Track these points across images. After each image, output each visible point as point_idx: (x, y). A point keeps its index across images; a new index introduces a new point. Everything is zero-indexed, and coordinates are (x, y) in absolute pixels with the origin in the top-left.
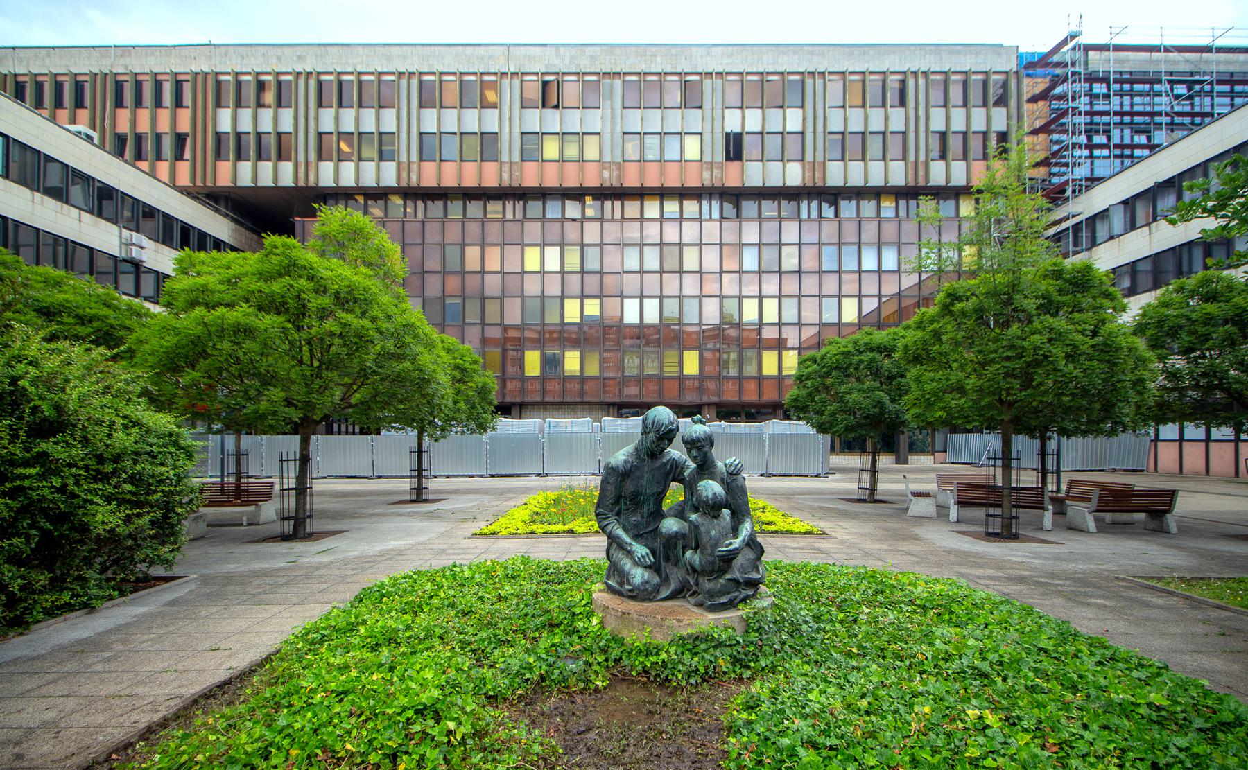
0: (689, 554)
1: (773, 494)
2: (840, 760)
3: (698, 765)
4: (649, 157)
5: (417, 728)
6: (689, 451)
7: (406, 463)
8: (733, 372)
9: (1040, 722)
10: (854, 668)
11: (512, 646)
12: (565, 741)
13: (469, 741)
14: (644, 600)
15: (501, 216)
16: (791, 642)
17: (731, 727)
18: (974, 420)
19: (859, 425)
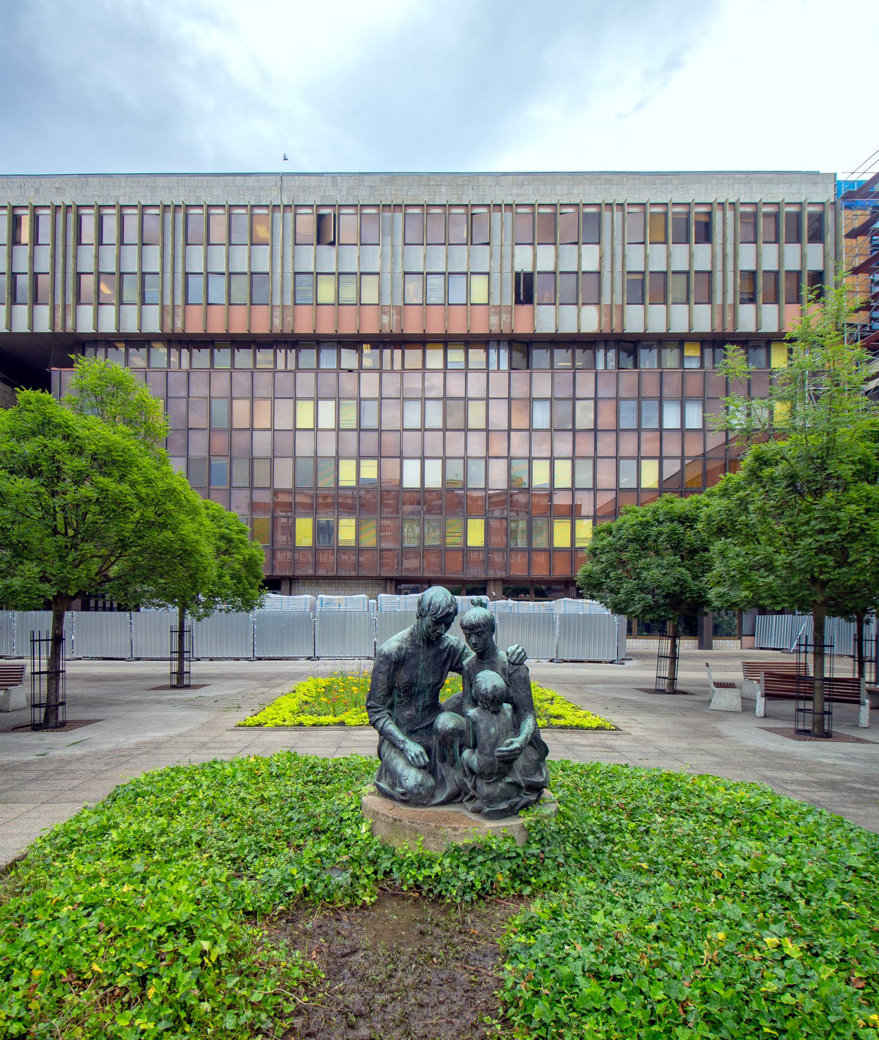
0: (466, 753)
1: (563, 682)
2: (625, 993)
3: (470, 994)
4: (432, 300)
5: (169, 947)
6: (468, 637)
7: (166, 644)
8: (521, 542)
9: (845, 952)
10: (644, 886)
11: (274, 855)
12: (328, 964)
13: (224, 963)
14: (417, 805)
15: (272, 366)
16: (575, 855)
17: (508, 952)
18: (783, 601)
19: (657, 606)
